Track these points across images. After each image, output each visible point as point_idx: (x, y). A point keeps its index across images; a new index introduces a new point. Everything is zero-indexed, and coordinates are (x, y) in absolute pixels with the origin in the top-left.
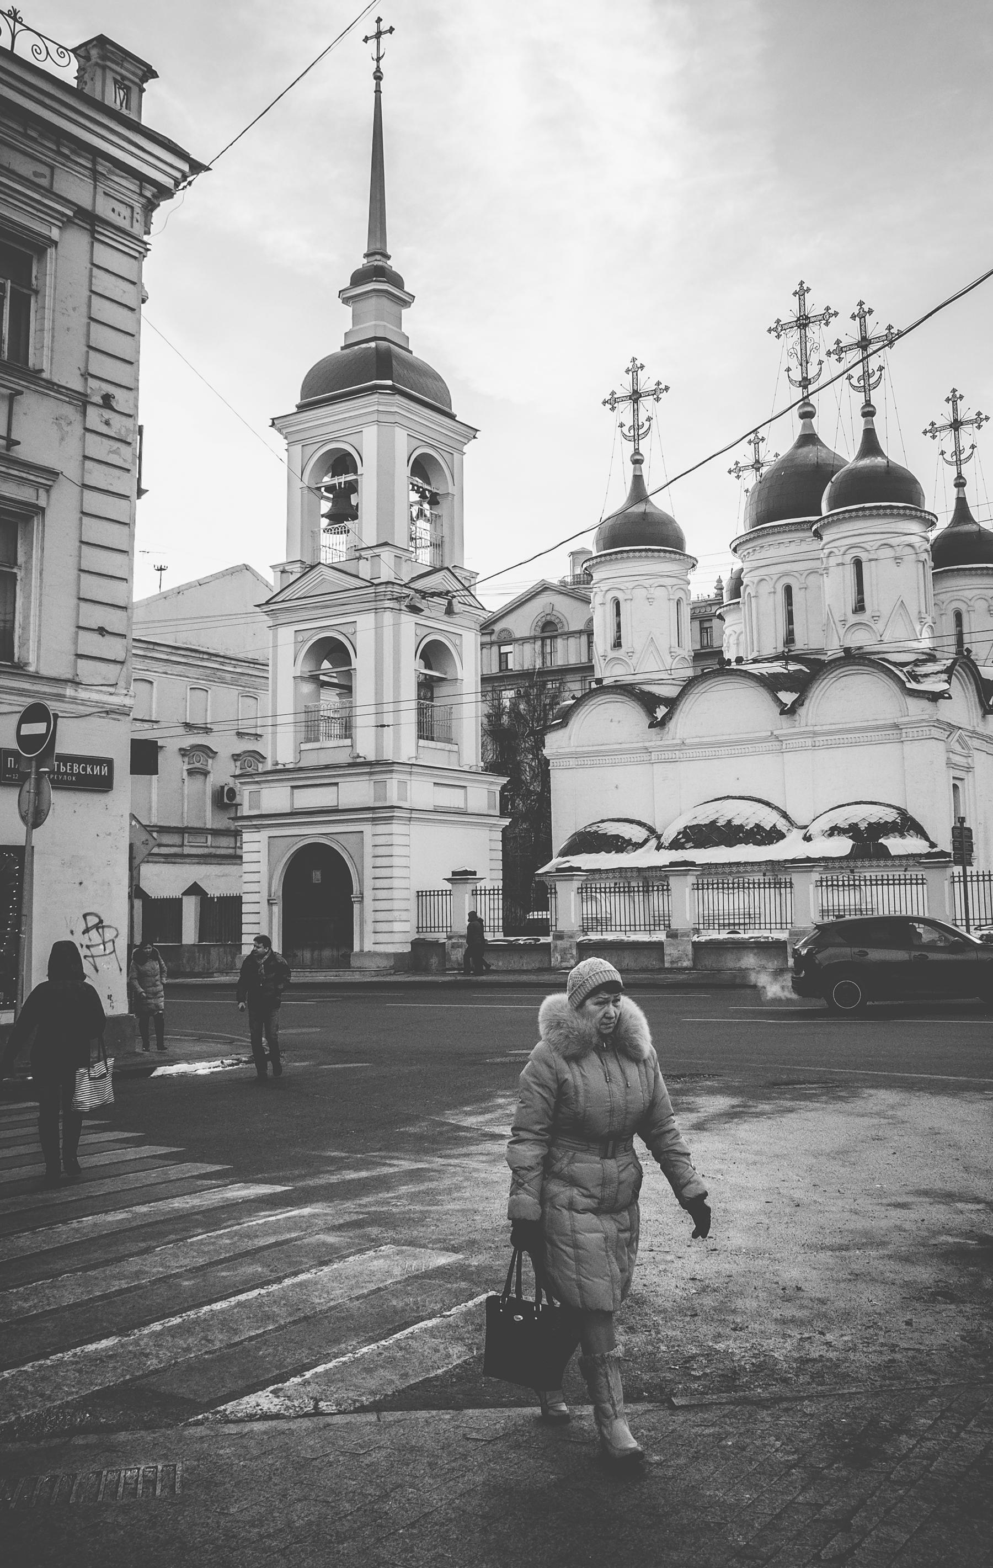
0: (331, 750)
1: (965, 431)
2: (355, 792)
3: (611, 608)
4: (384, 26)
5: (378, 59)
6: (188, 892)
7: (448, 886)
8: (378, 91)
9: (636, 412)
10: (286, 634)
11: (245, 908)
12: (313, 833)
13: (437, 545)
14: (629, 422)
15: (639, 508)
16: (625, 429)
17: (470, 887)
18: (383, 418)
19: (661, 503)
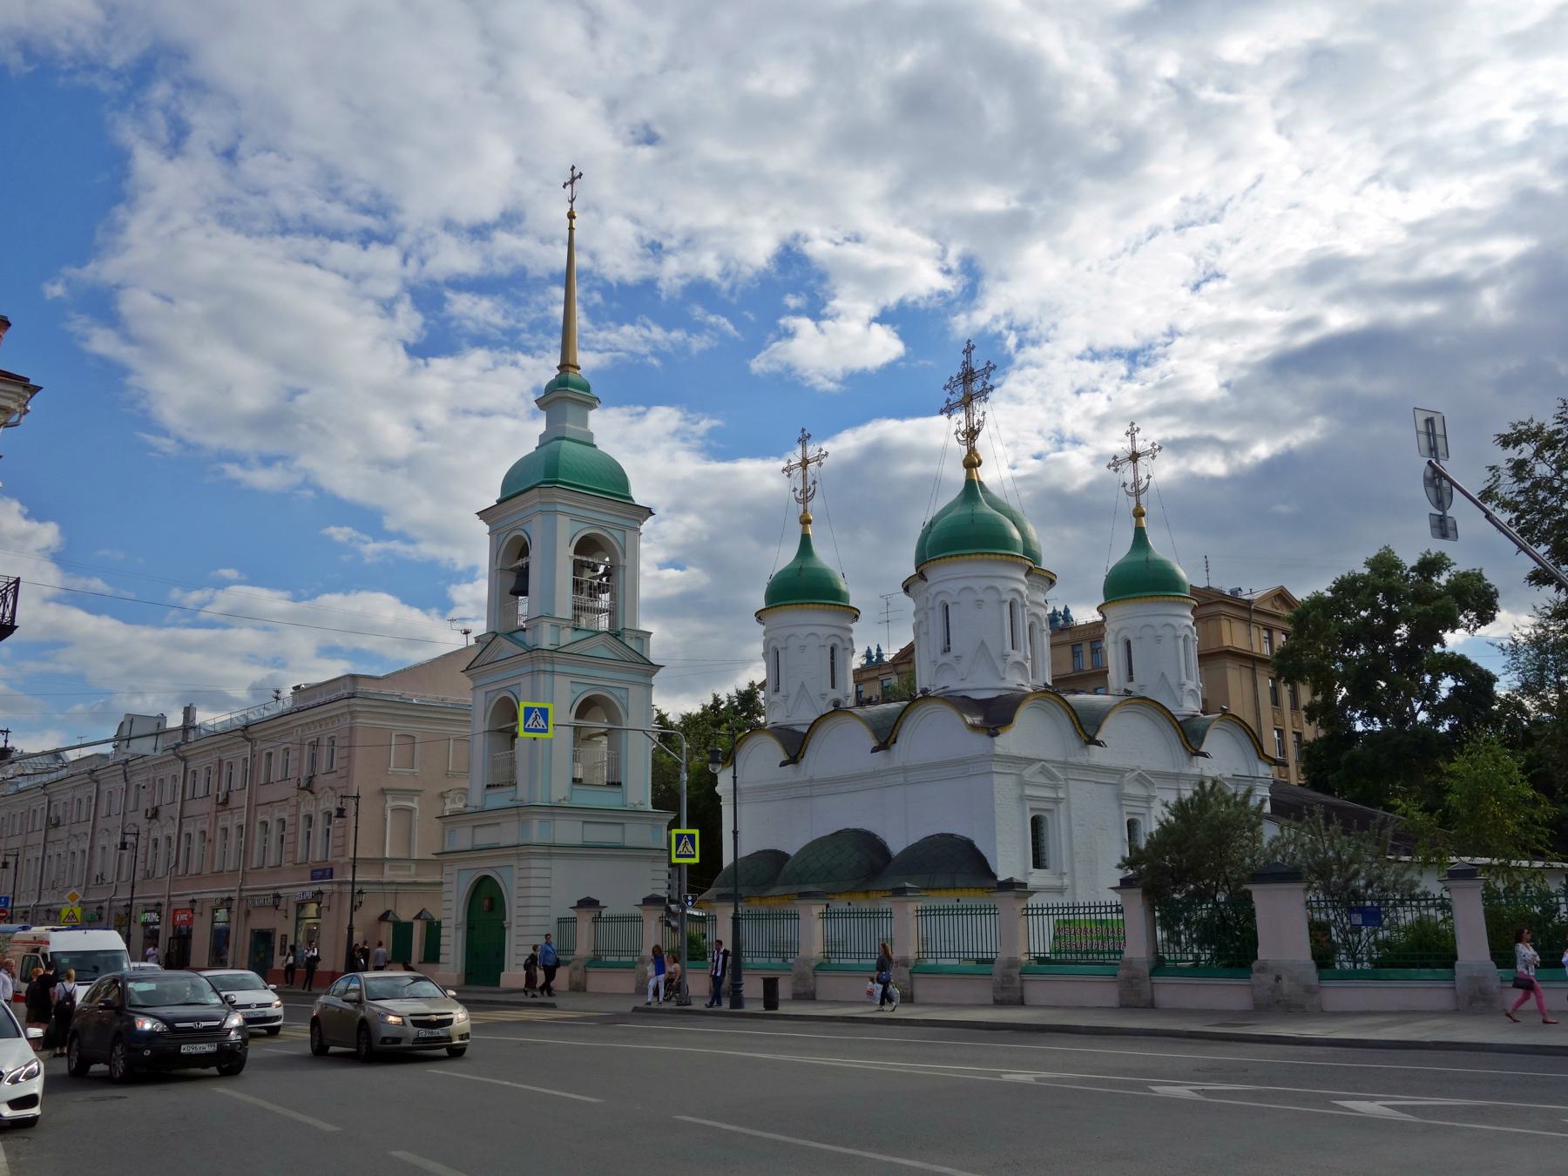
0: (500, 799)
1: (1142, 461)
2: (508, 834)
3: (1122, 648)
4: (576, 173)
5: (572, 202)
6: (418, 917)
7: (573, 914)
8: (571, 229)
9: (1135, 471)
10: (481, 694)
11: (443, 932)
12: (483, 867)
13: (612, 612)
14: (800, 487)
15: (1142, 558)
16: (1128, 488)
17: (1020, 906)
18: (545, 508)
19: (826, 556)
